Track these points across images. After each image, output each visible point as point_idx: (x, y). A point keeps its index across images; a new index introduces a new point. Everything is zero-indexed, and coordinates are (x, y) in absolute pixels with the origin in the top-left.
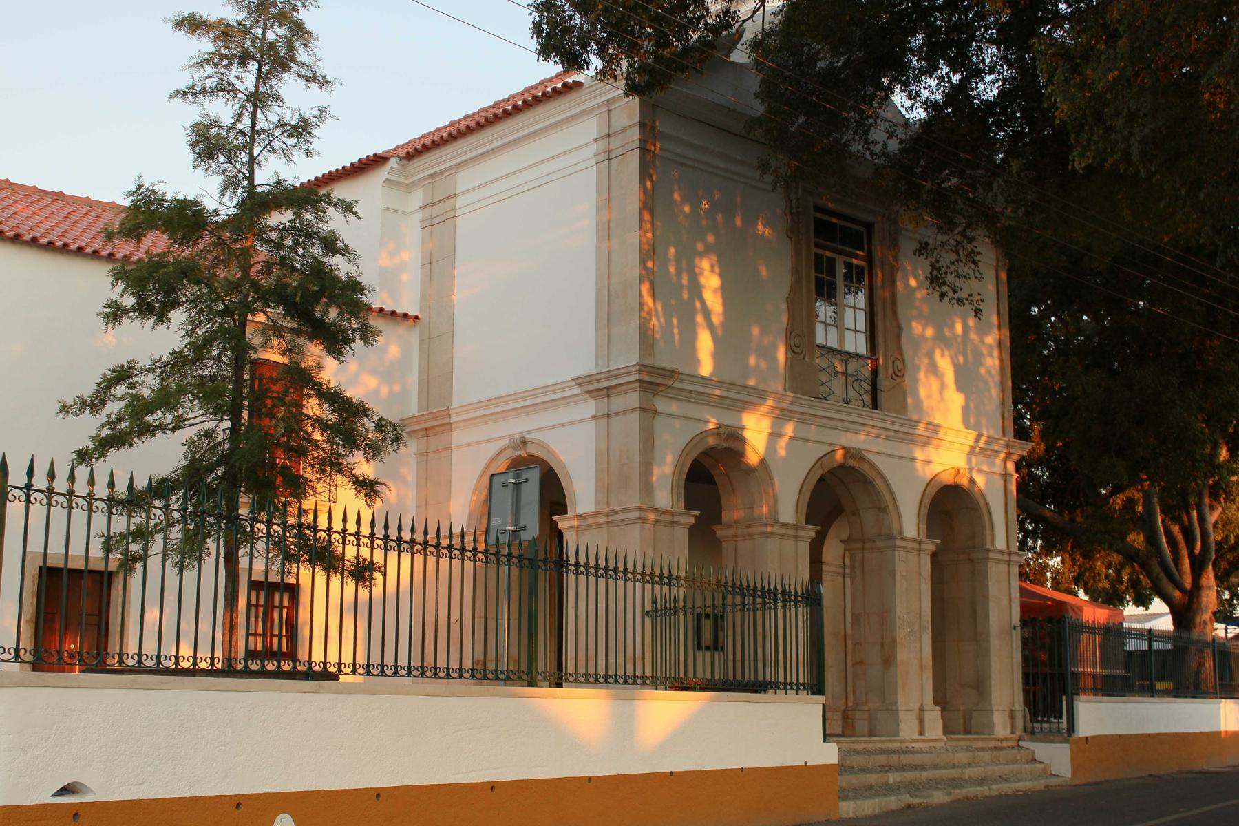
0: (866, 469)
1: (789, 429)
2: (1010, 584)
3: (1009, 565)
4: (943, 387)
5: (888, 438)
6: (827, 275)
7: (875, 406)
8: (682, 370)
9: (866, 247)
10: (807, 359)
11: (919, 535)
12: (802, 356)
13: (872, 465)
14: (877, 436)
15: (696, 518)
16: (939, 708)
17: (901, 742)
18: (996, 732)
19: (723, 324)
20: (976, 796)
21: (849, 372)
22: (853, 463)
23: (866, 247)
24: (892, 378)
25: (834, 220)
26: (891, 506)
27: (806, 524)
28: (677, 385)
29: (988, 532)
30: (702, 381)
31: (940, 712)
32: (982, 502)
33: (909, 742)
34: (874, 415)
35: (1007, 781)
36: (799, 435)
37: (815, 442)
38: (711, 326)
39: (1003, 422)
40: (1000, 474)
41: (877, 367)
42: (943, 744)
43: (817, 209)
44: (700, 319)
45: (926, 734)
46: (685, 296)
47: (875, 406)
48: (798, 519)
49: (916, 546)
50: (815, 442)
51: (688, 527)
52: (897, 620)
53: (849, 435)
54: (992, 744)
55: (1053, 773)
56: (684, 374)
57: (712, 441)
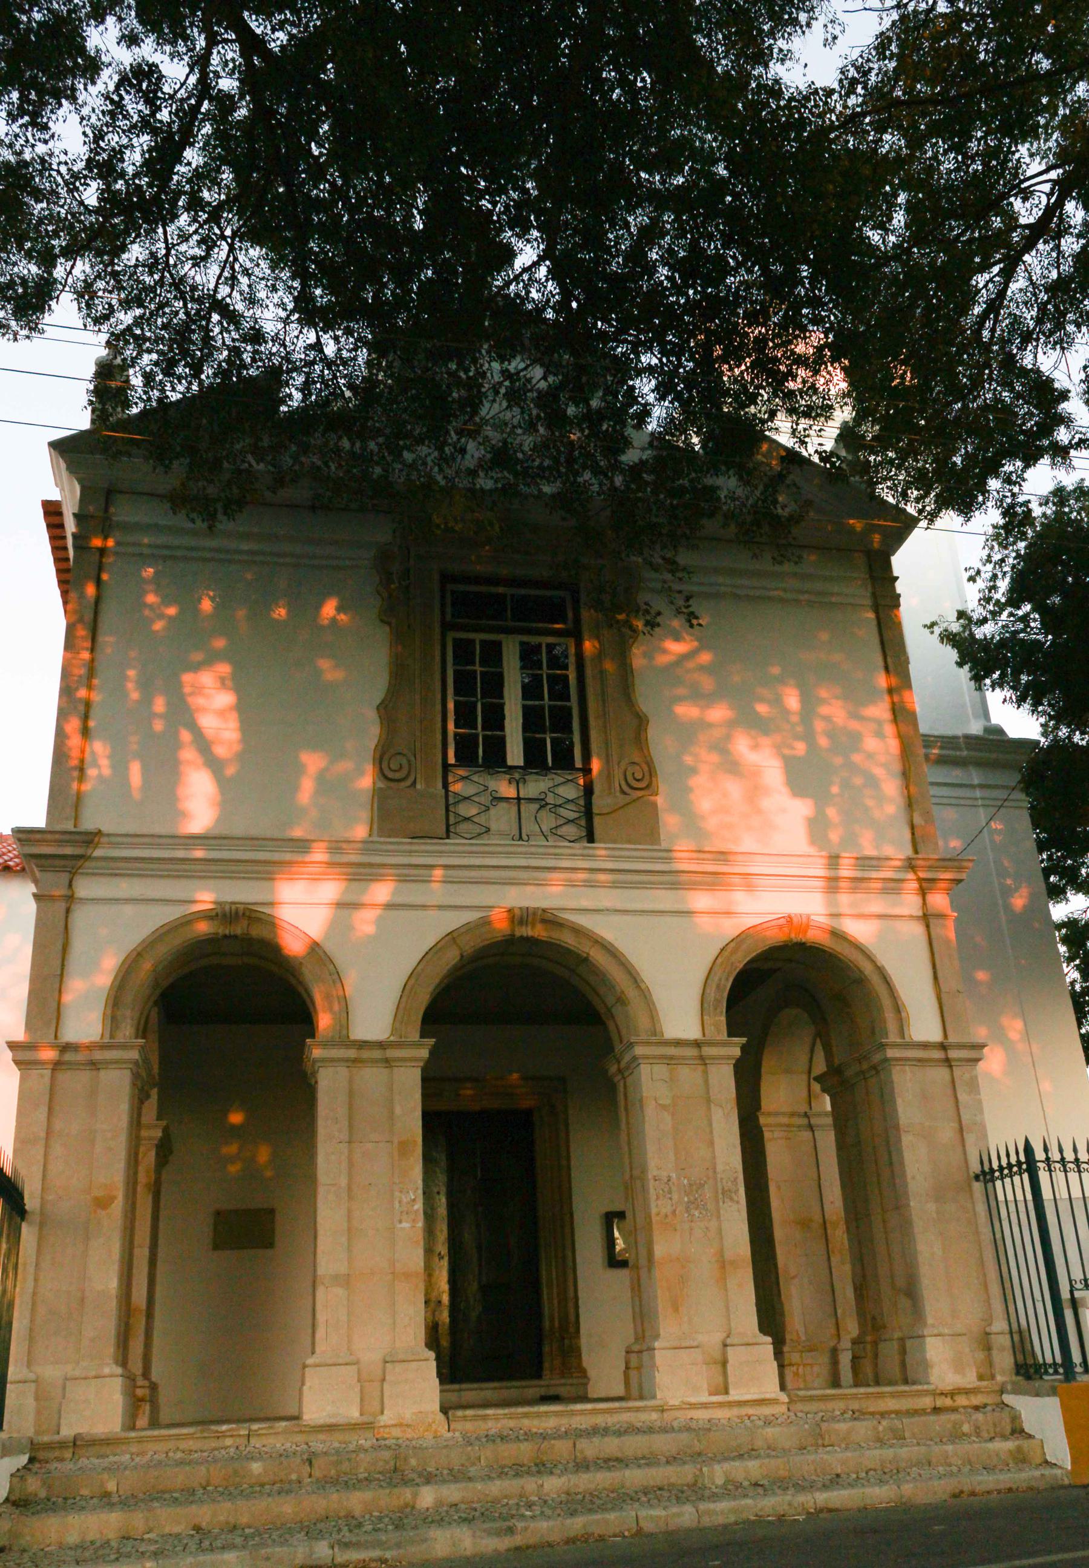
0: (568, 939)
1: (382, 892)
2: (956, 1098)
3: (951, 1067)
4: (755, 791)
5: (615, 885)
6: (481, 666)
7: (591, 838)
8: (105, 829)
9: (570, 615)
10: (418, 786)
11: (704, 1035)
12: (409, 782)
13: (578, 931)
14: (590, 884)
15: (743, 1048)
16: (769, 1339)
17: (662, 1410)
18: (933, 1379)
19: (241, 757)
20: (781, 1518)
21: (521, 796)
22: (238, 930)
23: (570, 615)
24: (623, 792)
25: (501, 590)
26: (631, 993)
27: (730, 1035)
28: (98, 853)
29: (889, 1016)
30: (38, 836)
31: (771, 1347)
32: (867, 969)
33: (680, 1408)
34: (520, 849)
35: (800, 1488)
36: (400, 900)
37: (440, 907)
38: (214, 764)
39: (913, 834)
40: (918, 918)
41: (591, 782)
42: (784, 1408)
43: (446, 578)
44: (189, 754)
45: (731, 1392)
46: (158, 726)
47: (591, 838)
48: (711, 1031)
49: (938, 1054)
50: (440, 907)
51: (734, 1062)
52: (652, 1183)
53: (530, 889)
54: (927, 1402)
55: (1049, 1459)
56: (108, 835)
57: (203, 928)
